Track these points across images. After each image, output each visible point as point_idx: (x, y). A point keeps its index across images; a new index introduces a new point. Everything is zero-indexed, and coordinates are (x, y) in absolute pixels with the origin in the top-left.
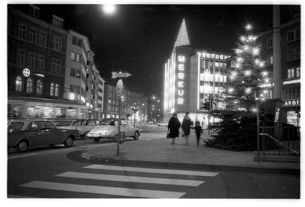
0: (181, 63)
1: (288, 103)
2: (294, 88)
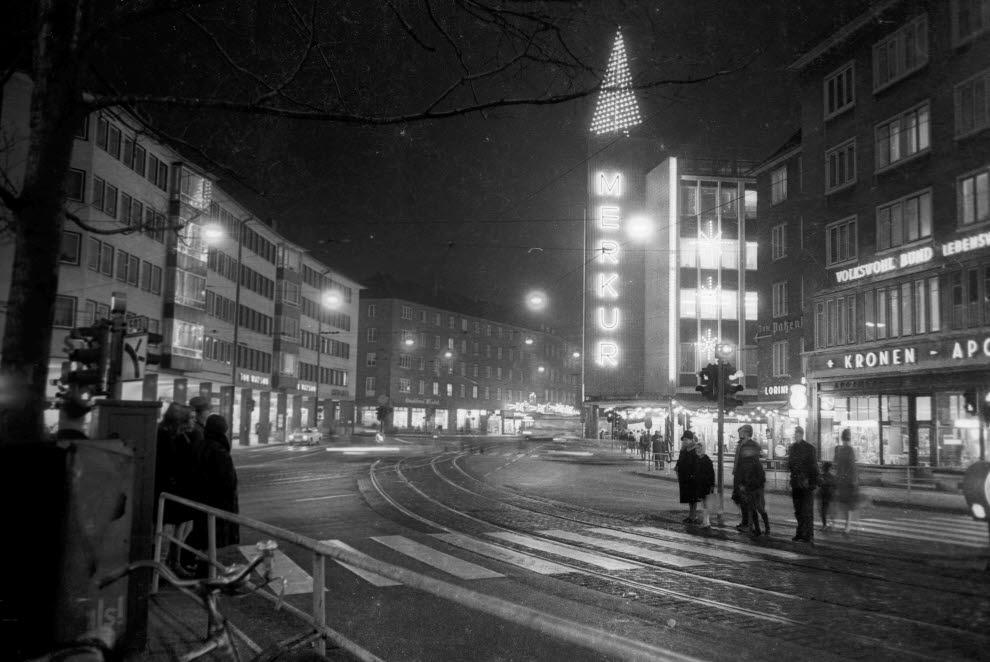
1: (964, 348)
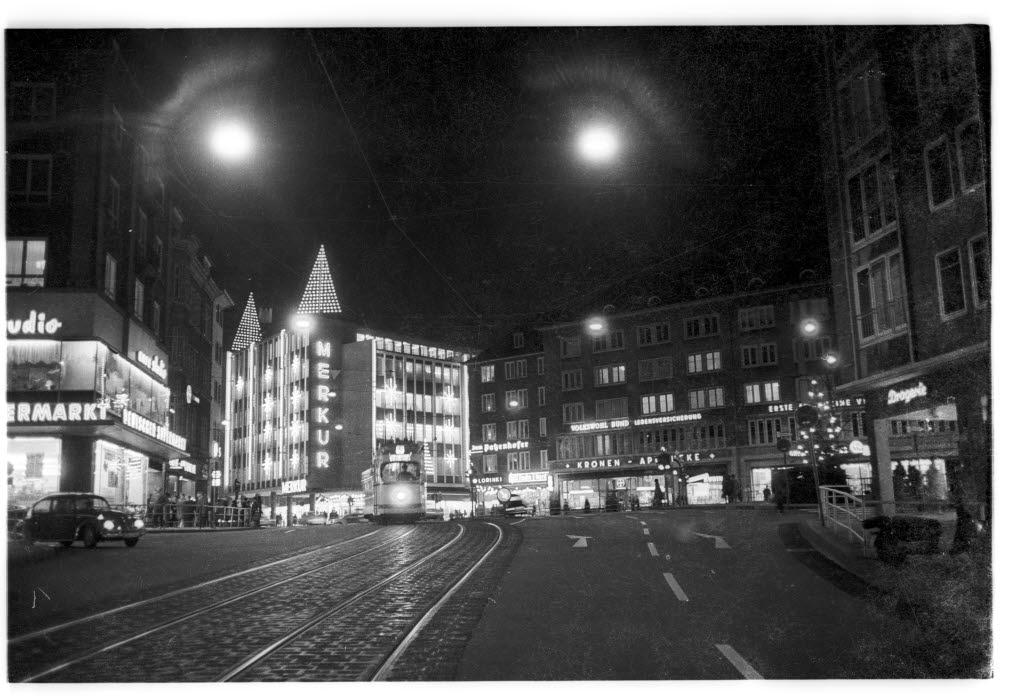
0: (323, 359)
1: (646, 460)
2: (665, 432)
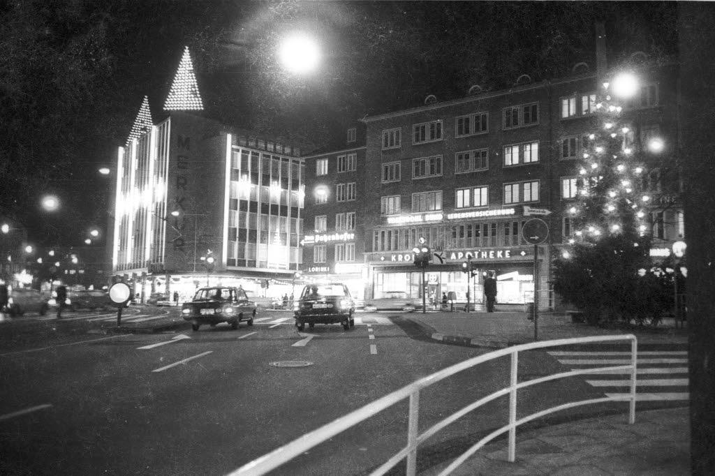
1: (457, 256)
